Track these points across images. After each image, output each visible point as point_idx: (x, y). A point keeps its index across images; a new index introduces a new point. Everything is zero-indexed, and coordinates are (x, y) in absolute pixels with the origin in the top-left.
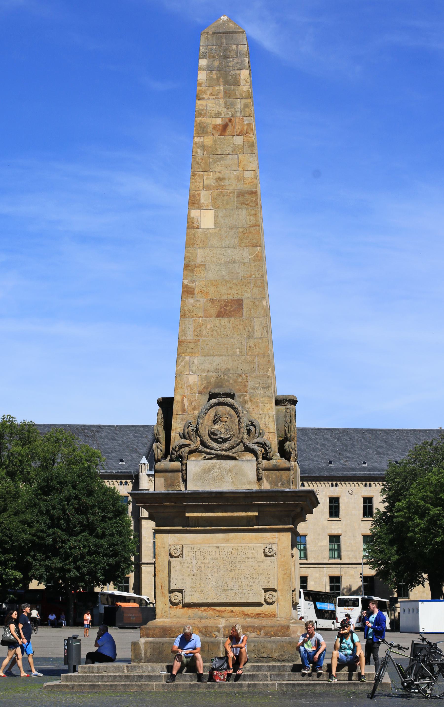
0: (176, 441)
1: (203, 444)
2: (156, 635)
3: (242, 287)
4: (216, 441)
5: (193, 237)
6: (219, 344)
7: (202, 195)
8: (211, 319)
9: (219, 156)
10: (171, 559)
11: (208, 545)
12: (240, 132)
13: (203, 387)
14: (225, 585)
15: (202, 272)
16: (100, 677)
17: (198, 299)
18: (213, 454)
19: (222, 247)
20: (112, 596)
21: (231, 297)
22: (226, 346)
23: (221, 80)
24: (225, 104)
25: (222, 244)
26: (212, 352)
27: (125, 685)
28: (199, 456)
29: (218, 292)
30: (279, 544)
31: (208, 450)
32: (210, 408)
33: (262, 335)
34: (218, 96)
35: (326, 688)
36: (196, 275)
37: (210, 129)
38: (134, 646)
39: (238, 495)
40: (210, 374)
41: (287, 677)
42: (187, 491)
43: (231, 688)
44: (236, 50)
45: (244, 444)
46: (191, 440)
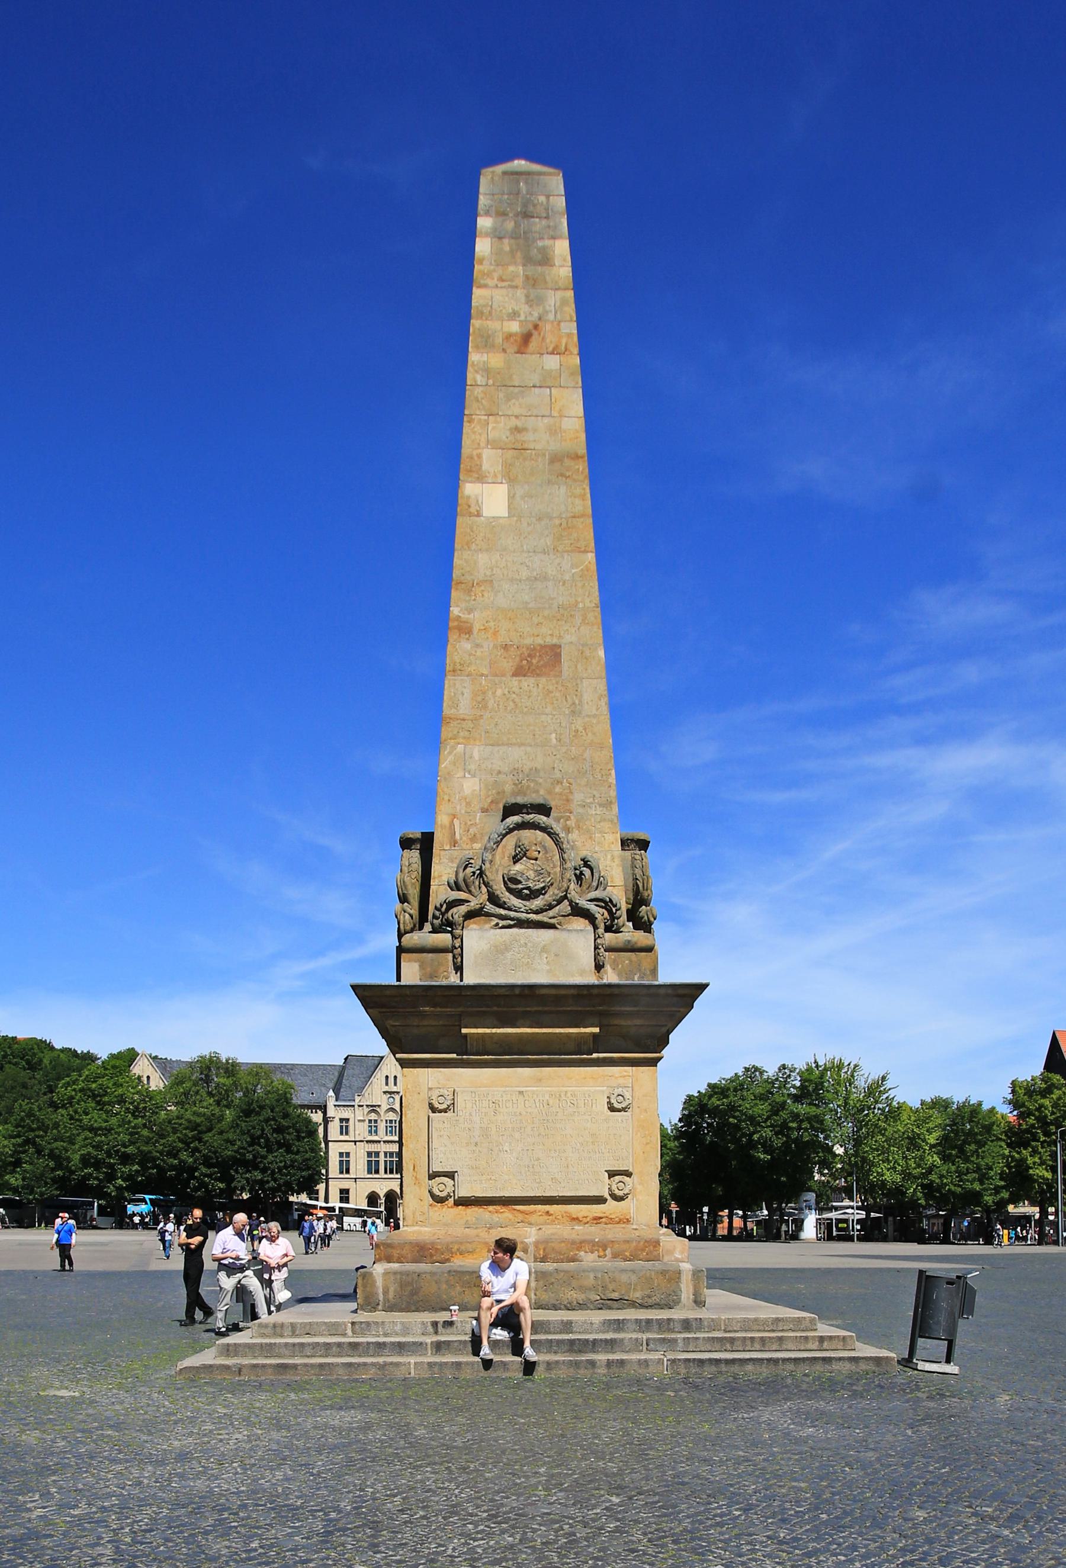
0: (439, 893)
1: (493, 899)
2: (405, 1258)
3: (560, 623)
4: (518, 894)
5: (469, 530)
6: (519, 724)
7: (484, 457)
8: (504, 679)
9: (516, 390)
10: (432, 1115)
11: (503, 1089)
12: (554, 349)
13: (489, 800)
14: (536, 1163)
15: (486, 595)
16: (297, 1348)
17: (478, 642)
18: (512, 919)
19: (523, 551)
20: (305, 1204)
21: (539, 641)
22: (532, 728)
23: (519, 254)
24: (527, 296)
25: (522, 546)
26: (505, 739)
27: (350, 1365)
28: (486, 922)
29: (516, 630)
30: (635, 1088)
31: (503, 912)
32: (507, 834)
33: (597, 710)
34: (514, 284)
35: (766, 1368)
36: (475, 600)
37: (499, 340)
38: (363, 1279)
39: (563, 992)
40: (502, 777)
41: (680, 1343)
42: (462, 984)
43: (572, 1370)
44: (545, 203)
45: (571, 902)
46: (470, 892)
